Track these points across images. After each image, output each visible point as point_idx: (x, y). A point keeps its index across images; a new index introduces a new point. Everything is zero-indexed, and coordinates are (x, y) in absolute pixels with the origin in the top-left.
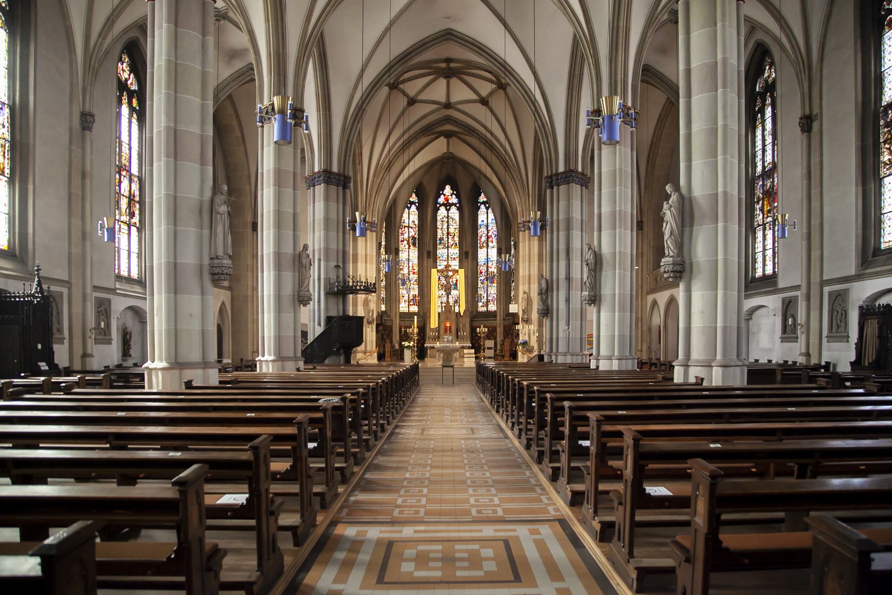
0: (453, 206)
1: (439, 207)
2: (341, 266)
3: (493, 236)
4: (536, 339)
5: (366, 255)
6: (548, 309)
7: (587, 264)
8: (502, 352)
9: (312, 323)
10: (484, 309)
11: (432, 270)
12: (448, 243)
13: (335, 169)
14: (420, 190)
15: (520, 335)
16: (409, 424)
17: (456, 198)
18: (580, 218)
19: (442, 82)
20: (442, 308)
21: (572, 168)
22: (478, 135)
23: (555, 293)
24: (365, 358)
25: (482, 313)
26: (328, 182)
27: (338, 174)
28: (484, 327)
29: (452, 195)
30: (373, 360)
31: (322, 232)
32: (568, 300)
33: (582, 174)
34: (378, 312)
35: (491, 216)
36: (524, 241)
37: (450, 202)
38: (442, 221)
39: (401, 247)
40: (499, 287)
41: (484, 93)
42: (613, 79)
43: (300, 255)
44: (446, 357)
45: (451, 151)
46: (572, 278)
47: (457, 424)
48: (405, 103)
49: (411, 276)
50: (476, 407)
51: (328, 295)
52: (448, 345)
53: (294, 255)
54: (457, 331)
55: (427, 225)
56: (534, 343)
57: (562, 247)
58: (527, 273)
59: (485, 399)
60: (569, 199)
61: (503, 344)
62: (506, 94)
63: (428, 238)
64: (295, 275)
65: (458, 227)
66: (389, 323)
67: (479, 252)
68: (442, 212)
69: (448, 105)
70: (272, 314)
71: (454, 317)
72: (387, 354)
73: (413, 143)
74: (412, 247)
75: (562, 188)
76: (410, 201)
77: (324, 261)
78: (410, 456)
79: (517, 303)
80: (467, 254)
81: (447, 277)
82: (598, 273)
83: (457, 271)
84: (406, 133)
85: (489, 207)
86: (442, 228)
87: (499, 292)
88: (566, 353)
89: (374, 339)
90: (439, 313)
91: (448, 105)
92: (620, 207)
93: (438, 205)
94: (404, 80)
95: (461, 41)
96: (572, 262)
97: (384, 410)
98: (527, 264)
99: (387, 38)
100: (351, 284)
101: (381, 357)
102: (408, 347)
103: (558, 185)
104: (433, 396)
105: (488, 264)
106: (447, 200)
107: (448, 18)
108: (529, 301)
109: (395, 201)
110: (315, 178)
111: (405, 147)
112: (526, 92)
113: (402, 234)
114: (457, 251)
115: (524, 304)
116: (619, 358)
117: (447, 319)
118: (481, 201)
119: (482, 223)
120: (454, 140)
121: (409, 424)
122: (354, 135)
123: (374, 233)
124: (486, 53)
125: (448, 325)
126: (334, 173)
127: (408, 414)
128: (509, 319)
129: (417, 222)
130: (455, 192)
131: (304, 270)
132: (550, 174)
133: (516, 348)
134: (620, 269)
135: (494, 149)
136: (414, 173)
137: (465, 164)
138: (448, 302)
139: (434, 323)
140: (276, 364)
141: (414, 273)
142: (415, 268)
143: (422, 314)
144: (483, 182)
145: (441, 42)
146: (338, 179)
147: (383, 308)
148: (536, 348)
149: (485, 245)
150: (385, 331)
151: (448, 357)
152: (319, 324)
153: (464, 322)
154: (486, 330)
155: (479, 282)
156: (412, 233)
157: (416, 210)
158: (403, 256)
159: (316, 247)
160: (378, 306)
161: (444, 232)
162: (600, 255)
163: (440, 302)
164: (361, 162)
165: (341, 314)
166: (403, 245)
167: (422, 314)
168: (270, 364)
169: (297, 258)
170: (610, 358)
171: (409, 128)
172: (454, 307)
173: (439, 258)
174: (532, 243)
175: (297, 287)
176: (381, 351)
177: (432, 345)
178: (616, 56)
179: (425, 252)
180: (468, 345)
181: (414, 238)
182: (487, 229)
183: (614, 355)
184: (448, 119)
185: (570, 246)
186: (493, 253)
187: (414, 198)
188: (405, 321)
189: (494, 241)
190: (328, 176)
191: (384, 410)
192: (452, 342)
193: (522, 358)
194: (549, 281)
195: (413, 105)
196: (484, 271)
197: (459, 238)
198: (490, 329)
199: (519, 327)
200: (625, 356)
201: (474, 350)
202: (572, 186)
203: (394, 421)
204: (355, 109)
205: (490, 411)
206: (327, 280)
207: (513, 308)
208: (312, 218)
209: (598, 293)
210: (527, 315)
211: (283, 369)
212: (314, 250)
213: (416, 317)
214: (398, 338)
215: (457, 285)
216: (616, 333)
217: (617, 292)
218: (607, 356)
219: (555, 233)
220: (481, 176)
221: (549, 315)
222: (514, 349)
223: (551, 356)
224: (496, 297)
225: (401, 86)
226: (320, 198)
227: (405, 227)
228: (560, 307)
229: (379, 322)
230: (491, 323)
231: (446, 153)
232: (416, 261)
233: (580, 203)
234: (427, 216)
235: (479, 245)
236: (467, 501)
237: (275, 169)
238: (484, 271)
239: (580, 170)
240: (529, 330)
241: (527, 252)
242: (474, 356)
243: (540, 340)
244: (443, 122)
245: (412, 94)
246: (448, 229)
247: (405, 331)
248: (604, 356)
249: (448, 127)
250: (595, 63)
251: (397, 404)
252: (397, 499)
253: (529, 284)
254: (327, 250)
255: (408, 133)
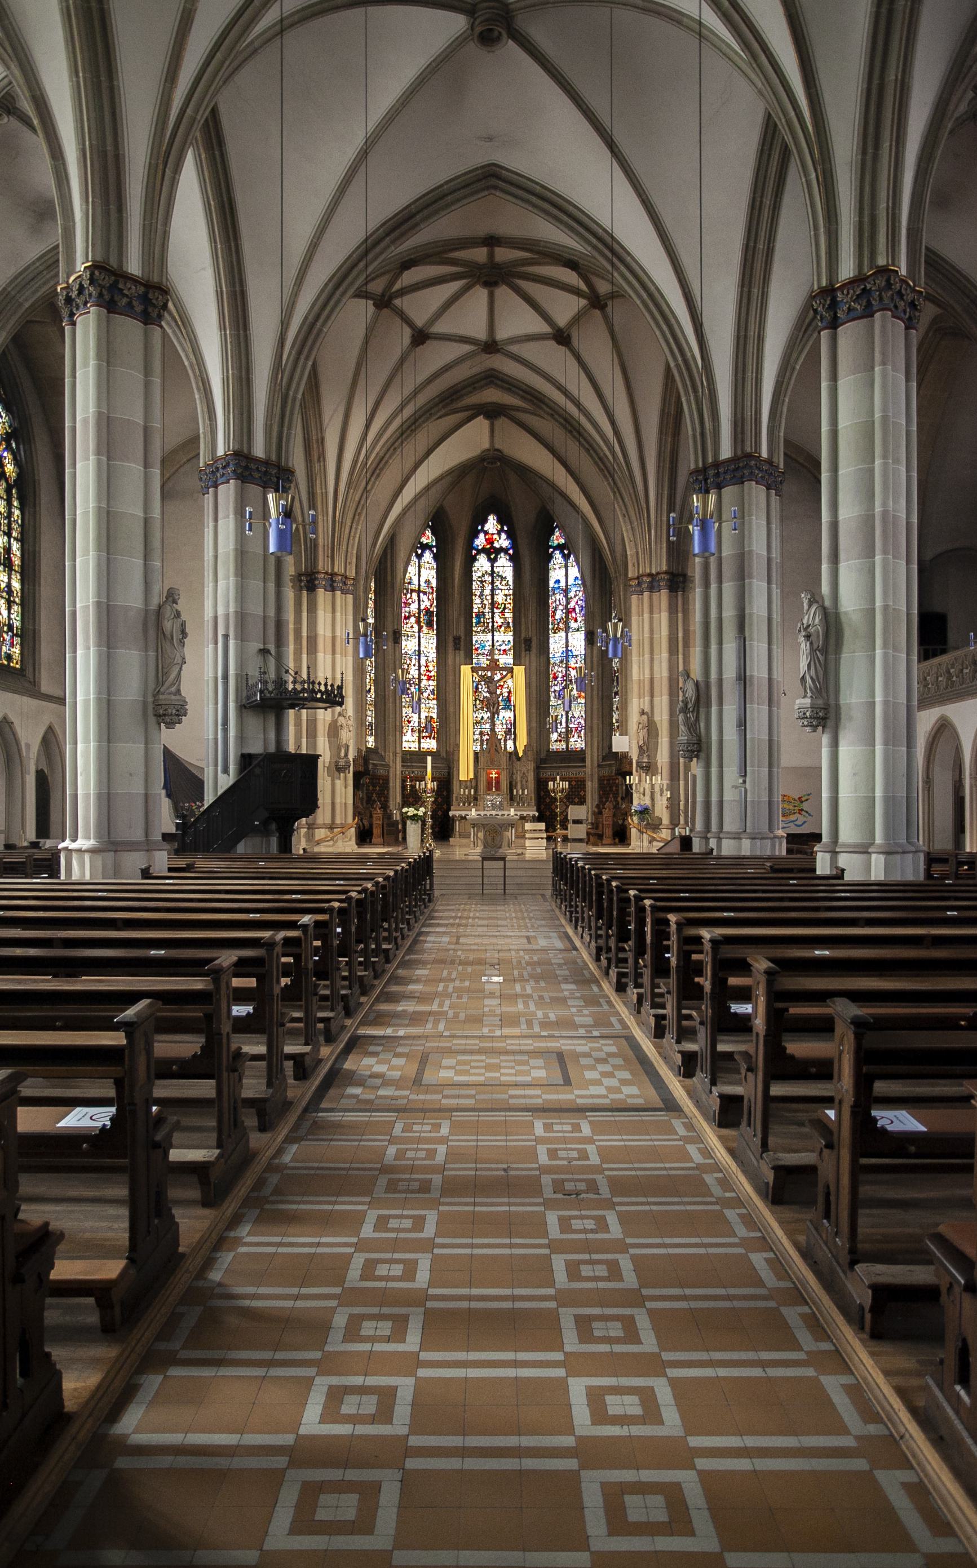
0: (502, 554)
1: (476, 555)
2: (273, 651)
3: (577, 610)
4: (665, 803)
5: (334, 638)
6: (699, 742)
7: (808, 637)
8: (597, 828)
9: (211, 768)
10: (562, 746)
11: (463, 667)
12: (493, 622)
13: (259, 451)
14: (438, 522)
15: (635, 795)
16: (389, 1031)
17: (508, 537)
18: (765, 553)
19: (481, 294)
20: (482, 745)
21: (748, 450)
22: (551, 408)
23: (714, 709)
24: (332, 839)
25: (557, 753)
26: (110, 305)
27: (266, 463)
28: (562, 779)
29: (499, 533)
30: (348, 845)
31: (232, 579)
32: (742, 724)
33: (769, 462)
34: (359, 751)
35: (574, 572)
36: (640, 614)
37: (496, 545)
38: (482, 582)
39: (406, 628)
40: (589, 706)
41: (562, 320)
42: (866, 212)
43: (159, 612)
44: (489, 839)
45: (497, 446)
46: (752, 677)
47: (515, 1031)
48: (407, 340)
49: (424, 683)
50: (560, 965)
51: (244, 710)
52: (494, 813)
53: (146, 611)
54: (511, 786)
55: (453, 587)
56: (661, 811)
57: (729, 613)
58: (647, 676)
59: (578, 943)
60: (741, 518)
61: (600, 813)
62: (606, 317)
63: (454, 612)
64: (147, 657)
65: (511, 592)
66: (382, 772)
67: (551, 640)
68: (482, 563)
69: (491, 347)
70: (92, 745)
71: (504, 760)
72: (377, 831)
73: (424, 422)
74: (425, 629)
75: (728, 492)
76: (421, 543)
77: (236, 639)
78: (353, 1222)
79: (624, 733)
80: (528, 642)
81: (489, 681)
82: (832, 657)
83: (511, 671)
84: (410, 401)
85: (569, 555)
86: (481, 595)
87: (589, 713)
88: (740, 833)
89: (350, 801)
90: (476, 754)
91: (491, 347)
92: (884, 504)
93: (474, 552)
94: (402, 289)
95: (520, 192)
96: (751, 645)
97: (410, 903)
98: (647, 656)
99: (360, 176)
100: (291, 687)
101: (364, 837)
102: (414, 818)
103: (719, 487)
104: (461, 930)
105: (568, 661)
106: (490, 541)
107: (490, 139)
108: (651, 728)
109: (392, 541)
110: (217, 469)
111: (409, 429)
112: (651, 296)
113: (408, 605)
114: (509, 637)
115: (641, 735)
116: (888, 850)
117: (492, 762)
118: (556, 543)
119: (556, 586)
120: (502, 422)
121: (389, 1031)
122: (298, 385)
123: (350, 597)
124: (570, 216)
125: (494, 776)
126: (256, 460)
127: (394, 988)
128: (610, 765)
129: (434, 583)
130: (505, 528)
131: (167, 646)
132: (700, 465)
133: (624, 820)
134: (885, 645)
135: (622, 261)
136: (428, 488)
137: (524, 472)
138: (493, 729)
139: (465, 771)
140: (99, 859)
141: (429, 678)
142: (431, 668)
143: (444, 754)
144: (559, 508)
145: (477, 192)
146: (266, 473)
147: (371, 741)
148: (666, 821)
149: (561, 625)
150: (374, 786)
151: (493, 839)
152: (226, 770)
153: (524, 769)
154: (566, 785)
155: (552, 695)
156: (426, 603)
157: (431, 560)
158: (409, 645)
159: (221, 611)
160: (361, 738)
161: (485, 602)
162: (837, 615)
163: (477, 732)
164: (322, 456)
165: (272, 749)
166: (409, 625)
167: (444, 754)
168: (87, 857)
169: (152, 618)
170: (864, 849)
171: (415, 393)
172: (505, 741)
173: (477, 649)
174: (656, 616)
175: (152, 685)
176: (366, 823)
177: (463, 813)
178: (876, 158)
179: (451, 639)
180: (531, 813)
181: (428, 612)
182: (566, 596)
183: (873, 844)
184: (492, 378)
185: (747, 611)
186: (578, 642)
187: (428, 538)
188: (413, 767)
189: (579, 619)
190: (244, 464)
191: (410, 903)
192: (501, 807)
193: (639, 843)
194: (702, 685)
195: (423, 343)
196: (560, 675)
197: (514, 612)
198: (573, 783)
199: (633, 780)
200: (900, 845)
201: (544, 824)
202: (750, 489)
203: (376, 982)
204: (299, 332)
205: (597, 982)
206: (242, 678)
207: (620, 743)
208: (211, 553)
209: (832, 702)
210: (648, 756)
211: (117, 872)
212: (216, 618)
213: (429, 758)
214: (399, 799)
215: (509, 701)
216: (879, 793)
217: (879, 698)
218: (855, 846)
219: (713, 587)
220: (556, 494)
221: (702, 755)
222: (620, 822)
223: (707, 839)
224: (583, 722)
225: (397, 302)
226: (228, 509)
227: (412, 591)
228: (725, 738)
229: (361, 769)
230: (575, 773)
231: (488, 450)
232: (433, 655)
233: (765, 523)
234: (453, 569)
235: (551, 626)
236: (543, 1270)
237: (99, 415)
238: (560, 675)
239: (764, 454)
240: (653, 786)
241: (647, 635)
242: (545, 835)
243: (673, 805)
244: (483, 383)
245: (420, 322)
246: (493, 595)
247: (413, 787)
248: (728, 833)
249: (492, 395)
250: (825, 178)
251: (415, 906)
252: (333, 1310)
253: (652, 696)
254: (242, 618)
255: (413, 402)
